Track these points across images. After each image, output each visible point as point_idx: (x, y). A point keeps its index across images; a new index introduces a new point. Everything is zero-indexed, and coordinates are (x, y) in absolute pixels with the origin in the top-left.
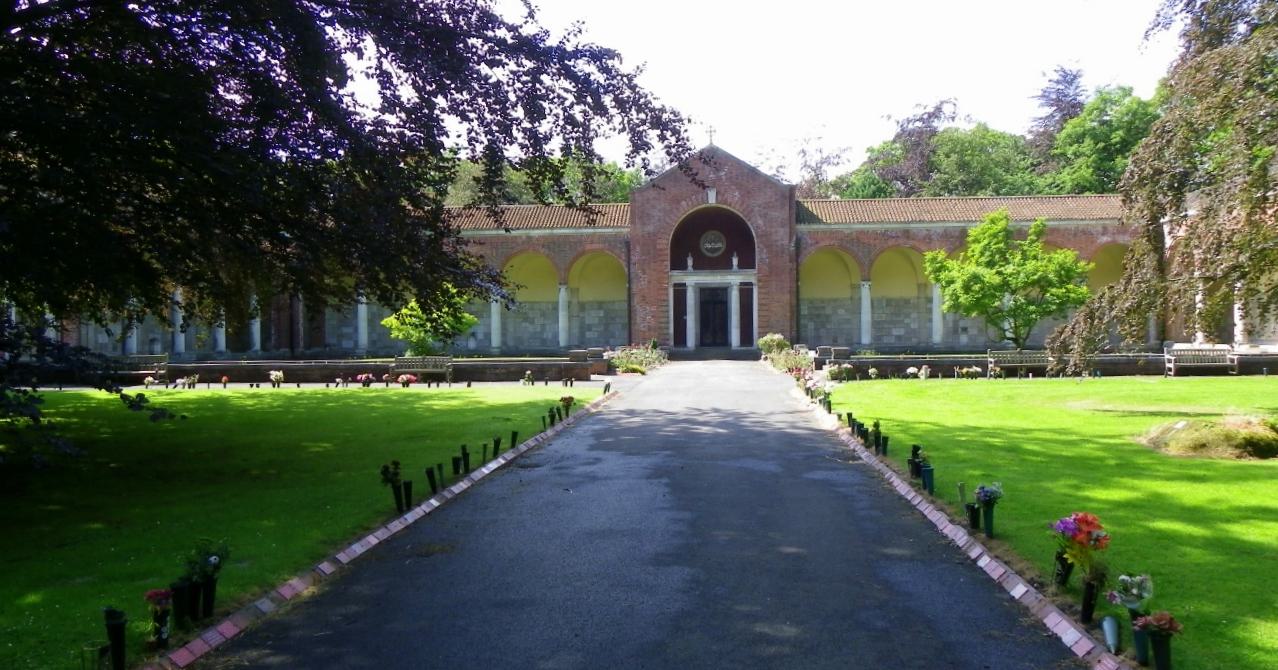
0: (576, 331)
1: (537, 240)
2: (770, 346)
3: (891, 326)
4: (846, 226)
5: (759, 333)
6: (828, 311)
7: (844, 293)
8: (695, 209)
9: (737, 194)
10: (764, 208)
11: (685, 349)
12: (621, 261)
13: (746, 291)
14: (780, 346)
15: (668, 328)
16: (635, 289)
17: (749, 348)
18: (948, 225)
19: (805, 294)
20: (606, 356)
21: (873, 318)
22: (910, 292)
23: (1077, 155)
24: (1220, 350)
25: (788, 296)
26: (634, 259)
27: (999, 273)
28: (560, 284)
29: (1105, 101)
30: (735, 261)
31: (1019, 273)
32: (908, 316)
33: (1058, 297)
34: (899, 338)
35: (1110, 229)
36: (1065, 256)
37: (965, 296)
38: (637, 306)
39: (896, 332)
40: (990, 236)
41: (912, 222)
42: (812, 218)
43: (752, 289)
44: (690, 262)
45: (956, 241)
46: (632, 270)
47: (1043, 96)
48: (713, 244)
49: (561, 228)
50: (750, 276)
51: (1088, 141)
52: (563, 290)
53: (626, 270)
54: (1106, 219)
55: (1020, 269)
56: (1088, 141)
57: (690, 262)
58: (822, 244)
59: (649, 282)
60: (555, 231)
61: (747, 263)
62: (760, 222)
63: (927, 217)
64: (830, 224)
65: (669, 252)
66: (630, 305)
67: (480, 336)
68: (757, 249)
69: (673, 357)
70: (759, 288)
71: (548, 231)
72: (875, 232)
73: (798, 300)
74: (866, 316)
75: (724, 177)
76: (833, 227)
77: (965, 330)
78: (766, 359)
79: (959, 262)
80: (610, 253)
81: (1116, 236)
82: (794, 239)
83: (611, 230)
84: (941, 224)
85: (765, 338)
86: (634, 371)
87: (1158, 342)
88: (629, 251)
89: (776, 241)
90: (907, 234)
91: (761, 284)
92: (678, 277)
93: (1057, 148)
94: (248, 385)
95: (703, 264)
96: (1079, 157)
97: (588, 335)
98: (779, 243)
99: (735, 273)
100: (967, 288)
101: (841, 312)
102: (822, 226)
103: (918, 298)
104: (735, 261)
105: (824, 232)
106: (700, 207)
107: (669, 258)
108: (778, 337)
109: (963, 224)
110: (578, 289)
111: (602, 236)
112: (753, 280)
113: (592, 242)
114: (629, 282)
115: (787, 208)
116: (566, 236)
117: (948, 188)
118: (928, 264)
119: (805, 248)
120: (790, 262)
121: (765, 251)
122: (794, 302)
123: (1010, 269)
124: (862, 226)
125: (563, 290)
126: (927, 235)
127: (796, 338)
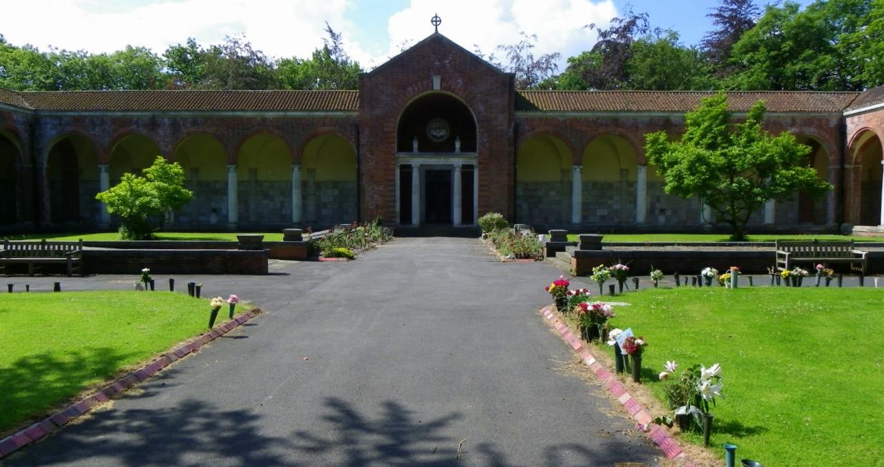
0: (312, 208)
1: (271, 121)
2: (490, 225)
4: (561, 114)
5: (479, 212)
8: (421, 95)
9: (460, 81)
10: (486, 95)
11: (411, 226)
12: (351, 143)
13: (467, 172)
14: (500, 226)
15: (394, 207)
16: (364, 169)
17: (470, 226)
18: (653, 114)
19: (522, 177)
20: (305, 237)
23: (752, 63)
26: (363, 141)
27: (724, 155)
28: (294, 163)
29: (775, 16)
30: (458, 145)
31: (745, 154)
32: (611, 198)
33: (787, 179)
34: (603, 218)
35: (798, 121)
37: (692, 178)
38: (367, 186)
40: (712, 118)
41: (621, 111)
42: (529, 106)
43: (473, 172)
44: (416, 145)
45: (674, 128)
46: (361, 152)
47: (717, 15)
48: (439, 132)
49: (294, 110)
50: (472, 159)
51: (762, 49)
52: (296, 169)
53: (356, 151)
54: (795, 111)
55: (746, 150)
56: (762, 49)
57: (416, 145)
59: (377, 163)
60: (289, 114)
61: (469, 147)
62: (481, 108)
63: (634, 108)
64: (546, 111)
65: (396, 135)
66: (359, 185)
67: (224, 212)
68: (478, 134)
69: (399, 233)
70: (480, 170)
71: (282, 113)
74: (577, 199)
75: (448, 65)
76: (548, 114)
77: (662, 211)
78: (486, 237)
79: (681, 143)
80: (341, 135)
81: (803, 127)
82: (513, 124)
83: (341, 113)
84: (647, 114)
85: (485, 217)
86: (339, 255)
87: (836, 224)
88: (358, 133)
89: (497, 126)
90: (616, 122)
91: (481, 166)
92: (404, 158)
93: (733, 57)
94: (84, 240)
95: (429, 147)
96: (754, 64)
97: (324, 211)
98: (499, 128)
99: (457, 156)
100: (692, 169)
101: (552, 194)
102: (539, 114)
103: (620, 182)
104: (458, 145)
105: (541, 119)
106: (425, 93)
107: (396, 141)
108: (497, 216)
109: (667, 114)
110: (314, 170)
111: (332, 119)
112: (474, 162)
113: (324, 125)
114: (359, 163)
115: (507, 95)
116: (300, 119)
117: (641, 87)
118: (648, 146)
121: (486, 135)
122: (512, 183)
123: (735, 150)
125: (296, 169)
126: (634, 124)
127: (512, 219)
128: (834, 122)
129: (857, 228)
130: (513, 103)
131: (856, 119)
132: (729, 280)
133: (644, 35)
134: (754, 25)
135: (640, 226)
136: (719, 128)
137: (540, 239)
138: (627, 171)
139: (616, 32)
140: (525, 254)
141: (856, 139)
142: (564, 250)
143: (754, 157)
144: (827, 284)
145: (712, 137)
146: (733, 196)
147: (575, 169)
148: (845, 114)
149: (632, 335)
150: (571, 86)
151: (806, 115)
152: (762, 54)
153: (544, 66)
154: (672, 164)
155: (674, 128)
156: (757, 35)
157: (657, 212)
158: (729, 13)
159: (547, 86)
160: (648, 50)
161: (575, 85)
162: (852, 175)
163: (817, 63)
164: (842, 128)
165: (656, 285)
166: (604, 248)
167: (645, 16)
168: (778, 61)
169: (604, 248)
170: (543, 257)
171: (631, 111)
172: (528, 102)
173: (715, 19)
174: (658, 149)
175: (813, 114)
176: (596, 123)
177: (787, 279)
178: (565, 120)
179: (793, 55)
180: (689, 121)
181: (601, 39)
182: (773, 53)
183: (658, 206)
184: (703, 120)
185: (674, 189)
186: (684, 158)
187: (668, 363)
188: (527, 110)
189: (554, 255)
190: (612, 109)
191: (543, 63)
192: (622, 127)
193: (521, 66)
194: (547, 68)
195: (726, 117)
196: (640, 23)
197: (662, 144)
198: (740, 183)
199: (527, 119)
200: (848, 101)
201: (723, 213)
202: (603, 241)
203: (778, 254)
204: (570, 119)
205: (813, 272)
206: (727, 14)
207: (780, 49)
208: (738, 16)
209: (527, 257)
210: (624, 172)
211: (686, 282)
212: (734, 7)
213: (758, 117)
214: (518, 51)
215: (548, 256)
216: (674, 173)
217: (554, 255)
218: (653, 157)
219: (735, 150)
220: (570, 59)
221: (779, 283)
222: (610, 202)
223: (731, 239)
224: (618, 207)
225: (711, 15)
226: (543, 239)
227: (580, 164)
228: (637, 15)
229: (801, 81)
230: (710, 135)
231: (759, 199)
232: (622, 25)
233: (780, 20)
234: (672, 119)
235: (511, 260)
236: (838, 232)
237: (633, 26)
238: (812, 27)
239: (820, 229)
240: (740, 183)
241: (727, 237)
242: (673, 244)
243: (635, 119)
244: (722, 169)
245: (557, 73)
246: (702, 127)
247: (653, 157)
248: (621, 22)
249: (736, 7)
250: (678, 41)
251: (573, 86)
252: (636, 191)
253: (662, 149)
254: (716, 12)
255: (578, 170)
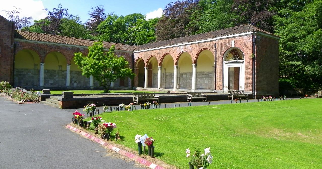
3: (49, 80)
4: (36, 42)
6: (25, 73)
7: (31, 67)
18: (73, 46)
19: (16, 66)
21: (44, 76)
22: (56, 68)
23: (104, 32)
24: (199, 93)
25: (10, 66)
31: (110, 63)
32: (55, 76)
34: (52, 84)
36: (122, 58)
39: (50, 82)
41: (61, 43)
42: (21, 37)
45: (85, 52)
47: (91, 14)
51: (107, 28)
55: (111, 61)
56: (107, 28)
58: (25, 47)
63: (66, 43)
72: (47, 45)
73: (14, 68)
74: (42, 76)
76: (30, 41)
77: (76, 82)
84: (71, 45)
87: (131, 87)
89: (5, 44)
90: (59, 47)
100: (93, 67)
103: (59, 70)
105: (27, 43)
109: (78, 46)
115: (11, 31)
119: (18, 48)
120: (11, 53)
123: (107, 61)
124: (42, 42)
128: (131, 54)
129: (138, 88)
130: (14, 35)
131: (137, 54)
132: (130, 108)
133: (66, 17)
134: (104, 20)
135: (67, 87)
136: (101, 53)
137: (37, 93)
138: (62, 66)
139: (55, 13)
140: (30, 100)
141: (137, 60)
142: (49, 98)
143: (113, 64)
144: (157, 108)
145: (99, 56)
146: (105, 77)
147: (68, 66)
148: (134, 52)
149: (148, 137)
150: (37, 31)
151: (123, 51)
152: (107, 30)
153: (24, 22)
154: (85, 65)
155: (85, 52)
156: (105, 23)
157: (73, 82)
158: (96, 14)
159: (26, 30)
160: (69, 22)
161: (39, 31)
162: (136, 71)
163: (124, 35)
164: (133, 57)
165: (104, 112)
166: (74, 97)
167: (66, 9)
168: (112, 33)
169: (74, 97)
170: (39, 101)
171: (65, 44)
172: (21, 35)
173: (91, 16)
174: (79, 59)
175: (125, 51)
176: (51, 47)
177: (145, 107)
178: (37, 45)
179: (117, 31)
180: (89, 50)
181: (49, 15)
182: (111, 30)
183: (73, 79)
184: (95, 50)
185: (86, 74)
186: (89, 63)
187: (187, 149)
188: (20, 39)
189: (45, 100)
190: (57, 42)
191: (24, 21)
192: (61, 49)
193: (14, 20)
194: (26, 22)
195: (102, 50)
196: (65, 12)
197: (81, 57)
198: (108, 73)
199: (20, 42)
200: (134, 48)
201: (102, 83)
202: (74, 94)
203: (134, 97)
204: (40, 44)
205: (153, 103)
206: (95, 15)
207: (112, 29)
208: (99, 16)
209: (31, 101)
210: (61, 66)
211: (114, 110)
212: (97, 13)
213: (113, 50)
214: (12, 14)
215: (42, 100)
216: (86, 68)
217: (45, 100)
218: (77, 62)
219: (107, 61)
220: (35, 21)
221: (143, 108)
222: (55, 78)
223: (105, 92)
224: (58, 80)
225: (90, 14)
226: (39, 93)
227: (44, 63)
228: (64, 9)
229: (118, 41)
230: (98, 55)
231: (114, 78)
232: (58, 11)
233: (112, 20)
234: (80, 48)
235: (23, 103)
236: (132, 89)
237: (62, 12)
238: (122, 24)
239: (127, 88)
240: (108, 73)
241: (103, 91)
242: (93, 95)
243: (66, 47)
244: (102, 67)
245: (30, 25)
246: (95, 52)
247: (77, 62)
248: (57, 10)
249: (98, 13)
250: (80, 21)
251: (38, 31)
252: (66, 74)
253: (81, 59)
254: (91, 13)
255: (43, 65)
